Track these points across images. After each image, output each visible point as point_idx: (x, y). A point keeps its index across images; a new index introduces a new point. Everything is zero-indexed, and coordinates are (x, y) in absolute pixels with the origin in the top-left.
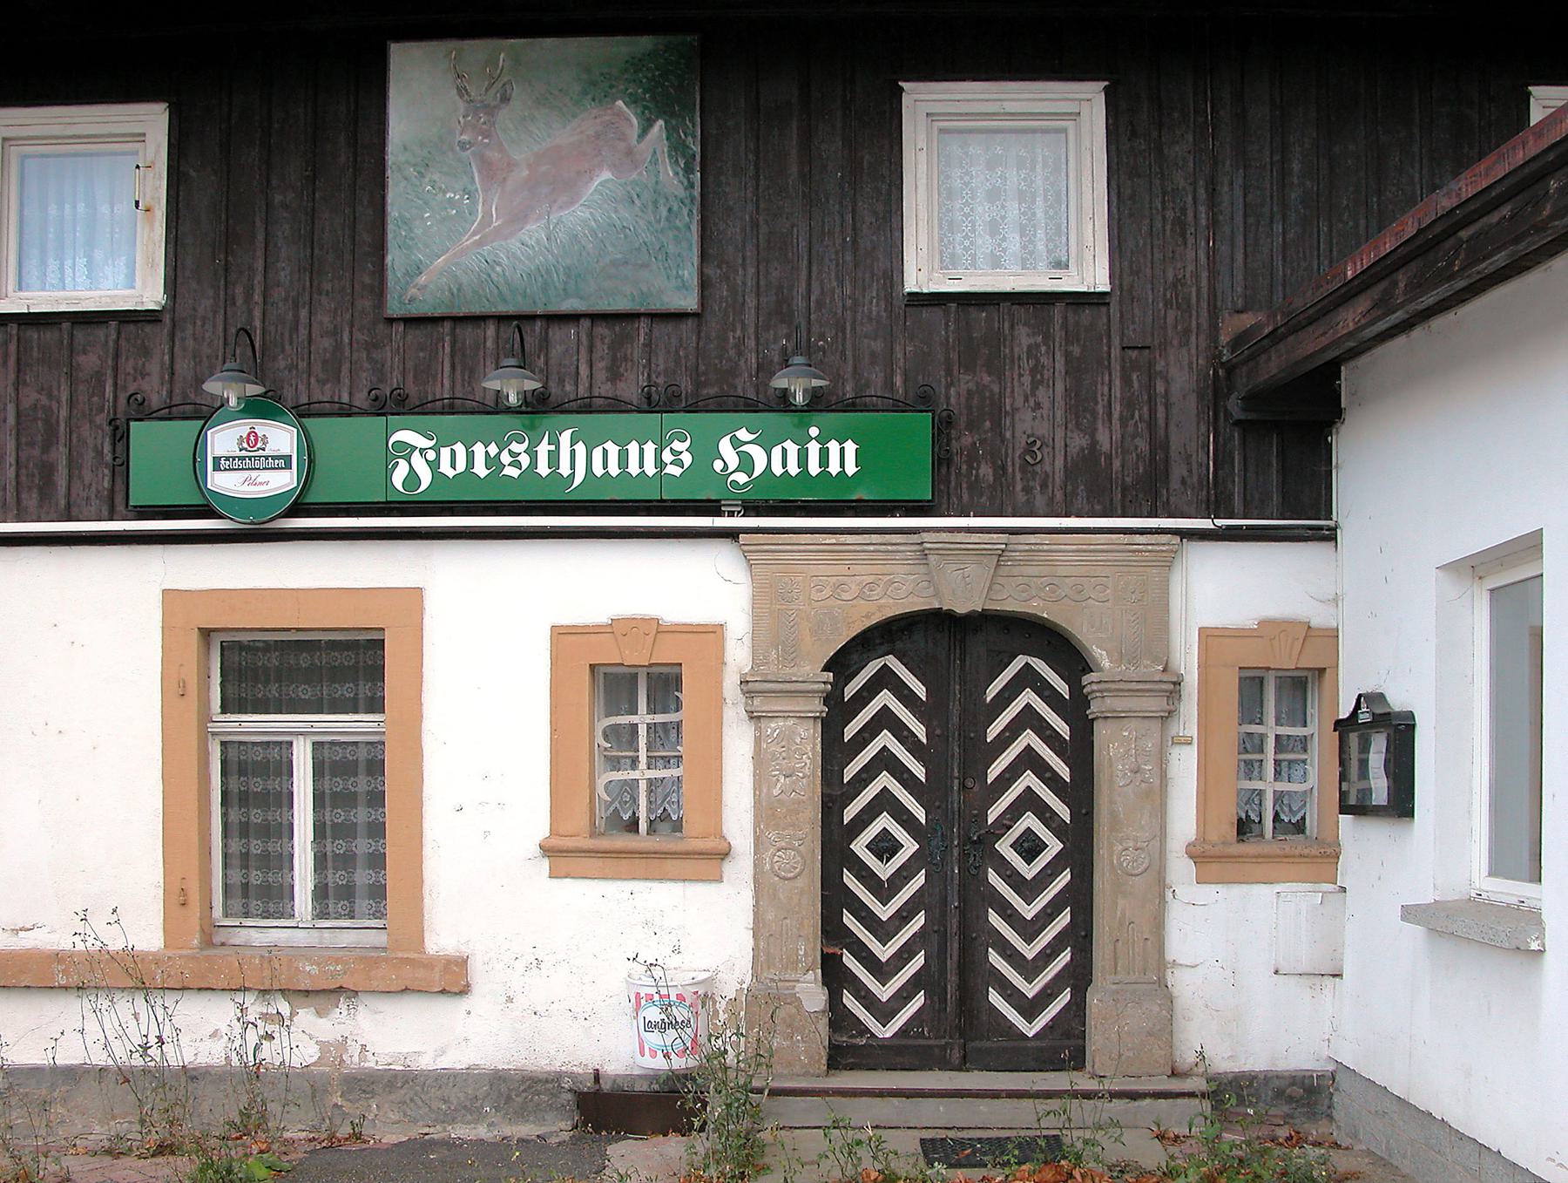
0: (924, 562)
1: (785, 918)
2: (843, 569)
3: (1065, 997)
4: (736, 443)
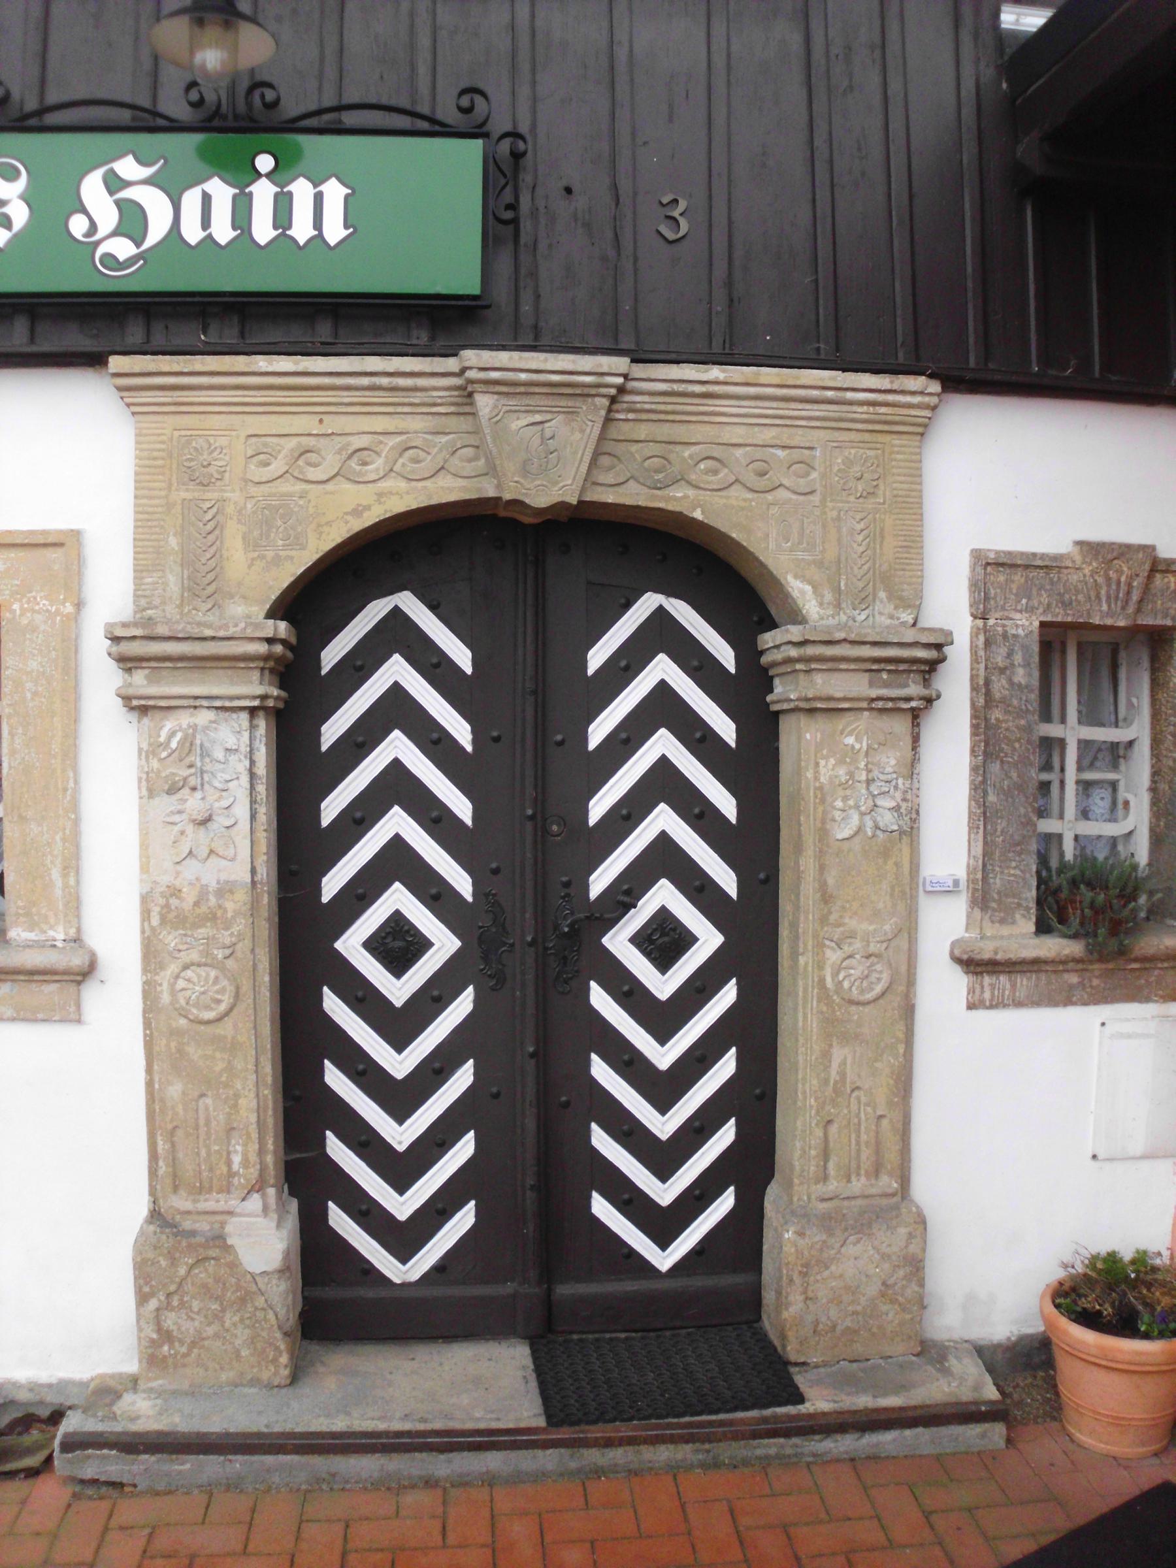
0: (467, 409)
1: (202, 1095)
2: (305, 423)
3: (726, 1203)
4: (114, 184)
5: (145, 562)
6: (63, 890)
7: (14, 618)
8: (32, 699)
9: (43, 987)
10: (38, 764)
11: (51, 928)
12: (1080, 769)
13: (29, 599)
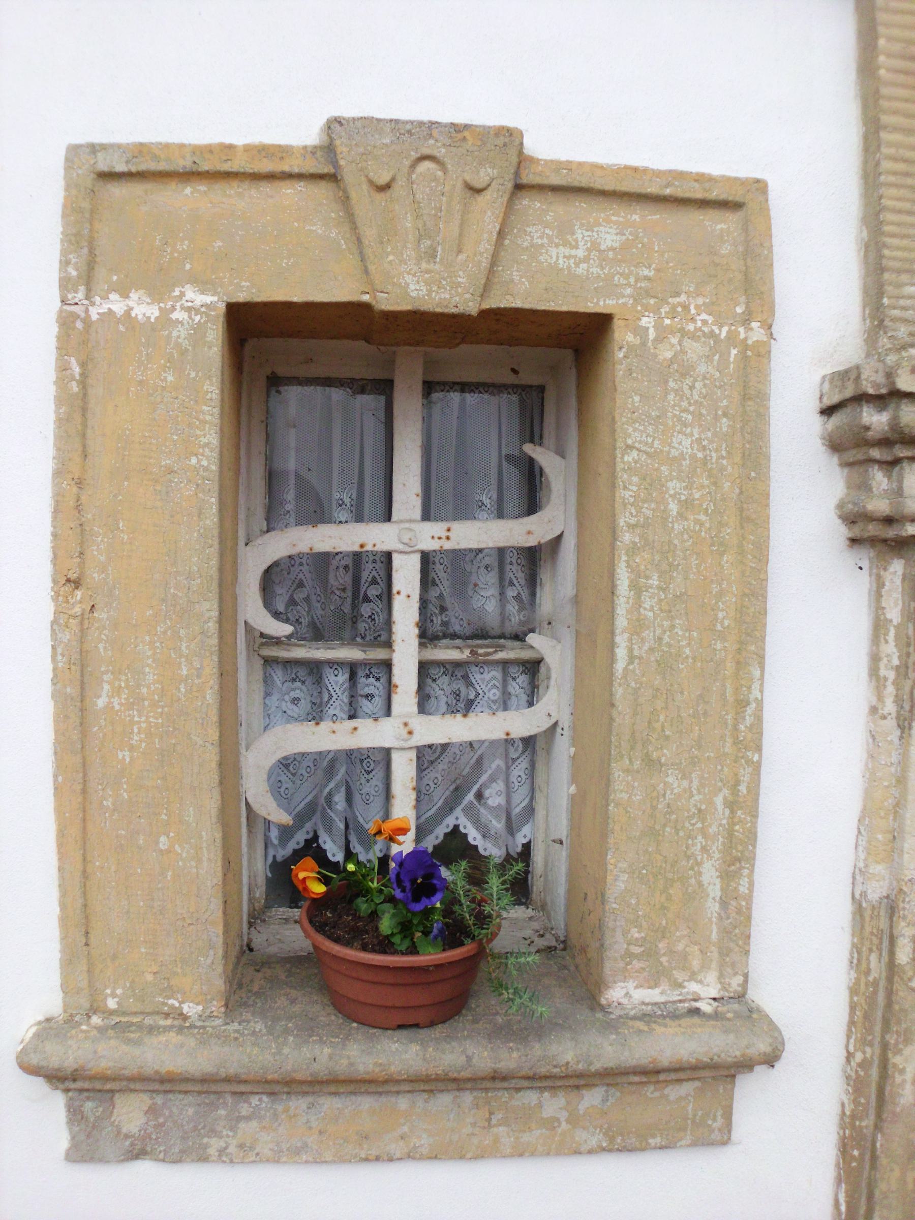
5: (906, 254)
6: (724, 904)
7: (644, 344)
8: (681, 516)
9: (666, 1091)
10: (687, 651)
11: (693, 977)
12: (426, 637)
13: (674, 308)
